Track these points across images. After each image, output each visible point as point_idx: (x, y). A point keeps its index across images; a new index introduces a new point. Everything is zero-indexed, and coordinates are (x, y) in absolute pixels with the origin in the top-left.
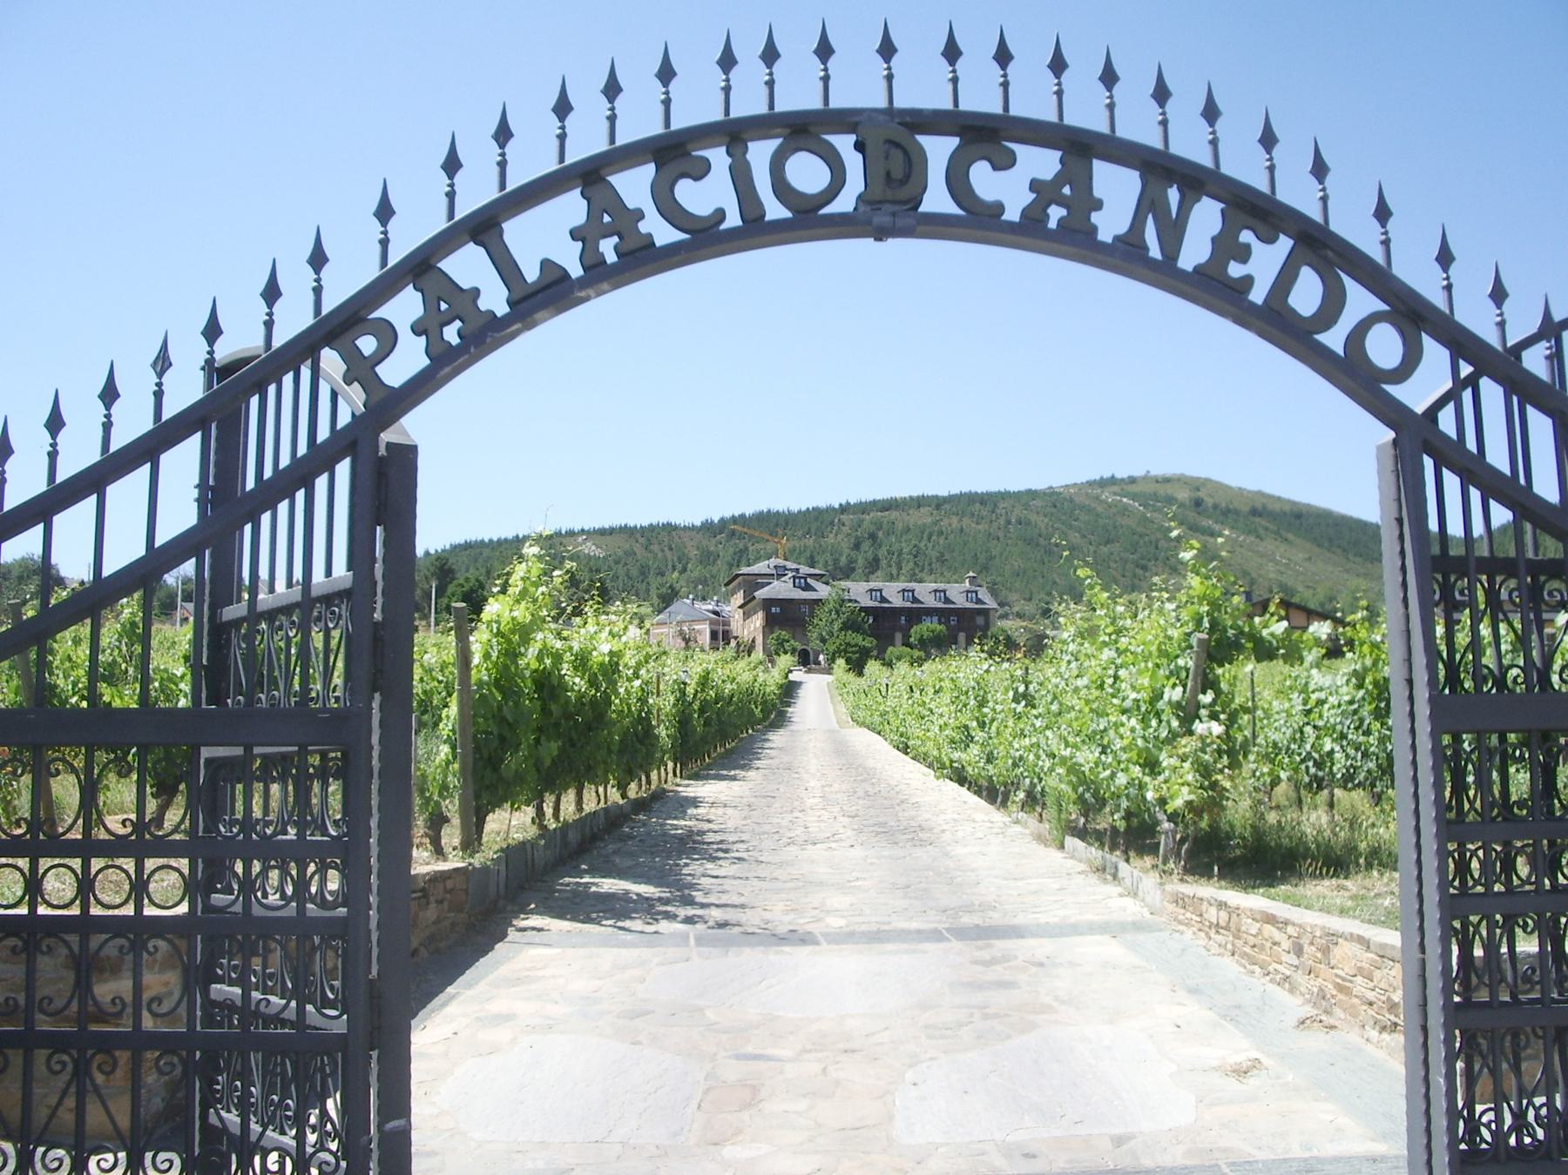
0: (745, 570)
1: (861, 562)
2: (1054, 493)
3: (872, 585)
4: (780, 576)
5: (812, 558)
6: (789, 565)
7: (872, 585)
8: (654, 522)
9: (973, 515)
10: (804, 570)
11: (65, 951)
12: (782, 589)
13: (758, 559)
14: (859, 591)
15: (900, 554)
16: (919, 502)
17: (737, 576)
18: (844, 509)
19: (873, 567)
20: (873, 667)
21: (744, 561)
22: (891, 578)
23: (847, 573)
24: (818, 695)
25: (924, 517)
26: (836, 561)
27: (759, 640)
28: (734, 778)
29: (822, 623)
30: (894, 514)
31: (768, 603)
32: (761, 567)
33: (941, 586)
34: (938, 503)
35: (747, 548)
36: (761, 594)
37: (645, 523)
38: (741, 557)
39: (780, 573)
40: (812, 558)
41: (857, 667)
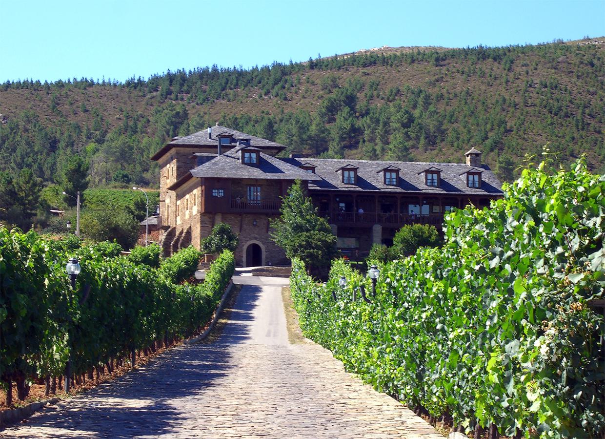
0: (181, 140)
1: (335, 133)
2: (454, 50)
3: (345, 162)
4: (224, 149)
5: (270, 125)
6: (237, 135)
7: (345, 162)
8: (64, 79)
9: (483, 75)
10: (258, 141)
11: (540, 402)
12: (227, 166)
13: (201, 126)
14: (329, 169)
15: (386, 124)
16: (416, 57)
17: (169, 148)
18: (314, 65)
19: (351, 140)
20: (340, 268)
21: (183, 127)
22: (374, 156)
23: (319, 148)
24: (274, 299)
25: (411, 80)
26: (303, 128)
27: (196, 232)
28: (195, 394)
29: (293, 212)
30: (378, 71)
31: (209, 184)
32: (201, 137)
33: (435, 165)
34: (441, 58)
35: (186, 114)
36: (200, 171)
37: (52, 79)
38: (178, 122)
39: (225, 144)
40: (270, 125)
41: (319, 271)
